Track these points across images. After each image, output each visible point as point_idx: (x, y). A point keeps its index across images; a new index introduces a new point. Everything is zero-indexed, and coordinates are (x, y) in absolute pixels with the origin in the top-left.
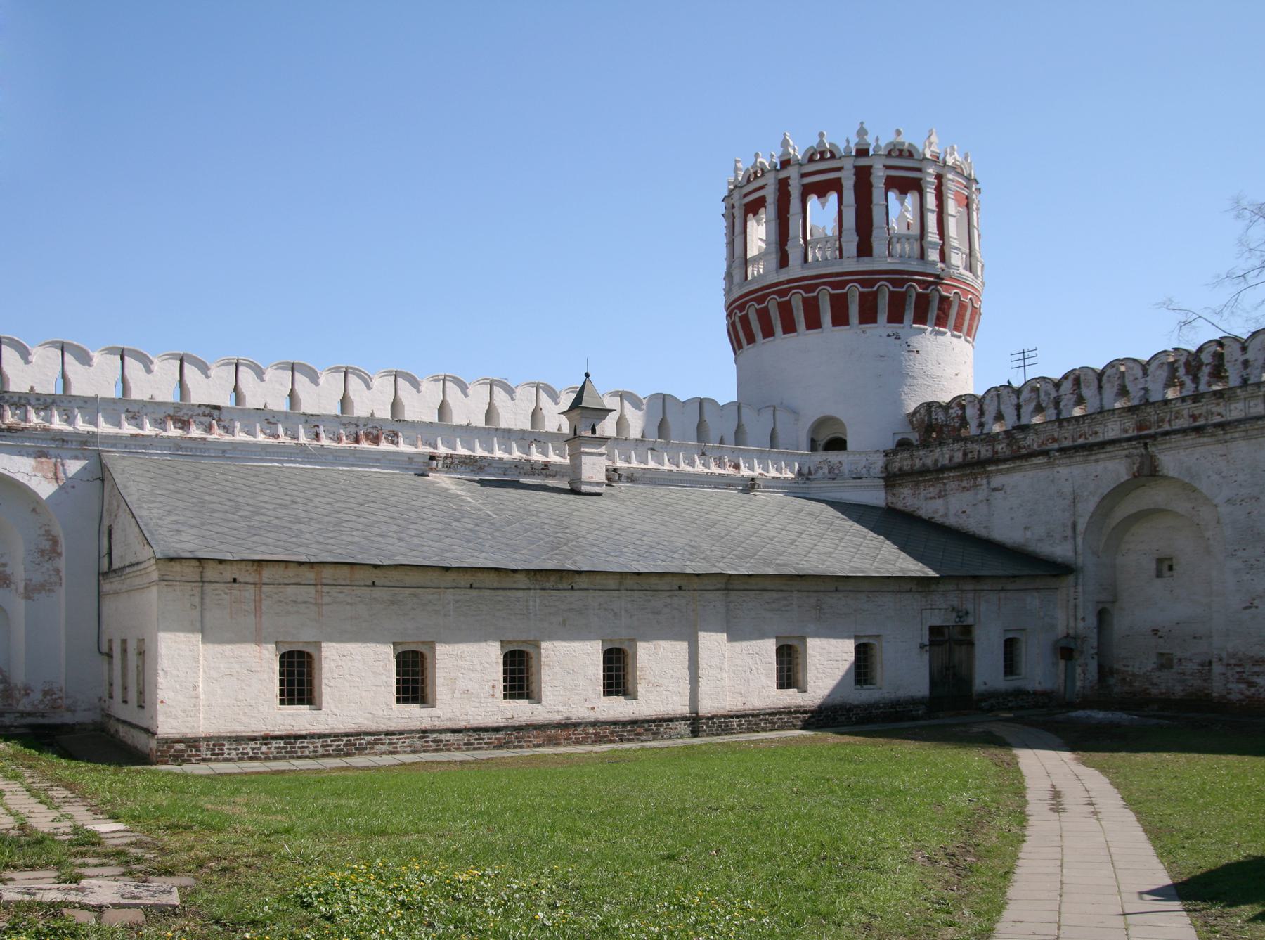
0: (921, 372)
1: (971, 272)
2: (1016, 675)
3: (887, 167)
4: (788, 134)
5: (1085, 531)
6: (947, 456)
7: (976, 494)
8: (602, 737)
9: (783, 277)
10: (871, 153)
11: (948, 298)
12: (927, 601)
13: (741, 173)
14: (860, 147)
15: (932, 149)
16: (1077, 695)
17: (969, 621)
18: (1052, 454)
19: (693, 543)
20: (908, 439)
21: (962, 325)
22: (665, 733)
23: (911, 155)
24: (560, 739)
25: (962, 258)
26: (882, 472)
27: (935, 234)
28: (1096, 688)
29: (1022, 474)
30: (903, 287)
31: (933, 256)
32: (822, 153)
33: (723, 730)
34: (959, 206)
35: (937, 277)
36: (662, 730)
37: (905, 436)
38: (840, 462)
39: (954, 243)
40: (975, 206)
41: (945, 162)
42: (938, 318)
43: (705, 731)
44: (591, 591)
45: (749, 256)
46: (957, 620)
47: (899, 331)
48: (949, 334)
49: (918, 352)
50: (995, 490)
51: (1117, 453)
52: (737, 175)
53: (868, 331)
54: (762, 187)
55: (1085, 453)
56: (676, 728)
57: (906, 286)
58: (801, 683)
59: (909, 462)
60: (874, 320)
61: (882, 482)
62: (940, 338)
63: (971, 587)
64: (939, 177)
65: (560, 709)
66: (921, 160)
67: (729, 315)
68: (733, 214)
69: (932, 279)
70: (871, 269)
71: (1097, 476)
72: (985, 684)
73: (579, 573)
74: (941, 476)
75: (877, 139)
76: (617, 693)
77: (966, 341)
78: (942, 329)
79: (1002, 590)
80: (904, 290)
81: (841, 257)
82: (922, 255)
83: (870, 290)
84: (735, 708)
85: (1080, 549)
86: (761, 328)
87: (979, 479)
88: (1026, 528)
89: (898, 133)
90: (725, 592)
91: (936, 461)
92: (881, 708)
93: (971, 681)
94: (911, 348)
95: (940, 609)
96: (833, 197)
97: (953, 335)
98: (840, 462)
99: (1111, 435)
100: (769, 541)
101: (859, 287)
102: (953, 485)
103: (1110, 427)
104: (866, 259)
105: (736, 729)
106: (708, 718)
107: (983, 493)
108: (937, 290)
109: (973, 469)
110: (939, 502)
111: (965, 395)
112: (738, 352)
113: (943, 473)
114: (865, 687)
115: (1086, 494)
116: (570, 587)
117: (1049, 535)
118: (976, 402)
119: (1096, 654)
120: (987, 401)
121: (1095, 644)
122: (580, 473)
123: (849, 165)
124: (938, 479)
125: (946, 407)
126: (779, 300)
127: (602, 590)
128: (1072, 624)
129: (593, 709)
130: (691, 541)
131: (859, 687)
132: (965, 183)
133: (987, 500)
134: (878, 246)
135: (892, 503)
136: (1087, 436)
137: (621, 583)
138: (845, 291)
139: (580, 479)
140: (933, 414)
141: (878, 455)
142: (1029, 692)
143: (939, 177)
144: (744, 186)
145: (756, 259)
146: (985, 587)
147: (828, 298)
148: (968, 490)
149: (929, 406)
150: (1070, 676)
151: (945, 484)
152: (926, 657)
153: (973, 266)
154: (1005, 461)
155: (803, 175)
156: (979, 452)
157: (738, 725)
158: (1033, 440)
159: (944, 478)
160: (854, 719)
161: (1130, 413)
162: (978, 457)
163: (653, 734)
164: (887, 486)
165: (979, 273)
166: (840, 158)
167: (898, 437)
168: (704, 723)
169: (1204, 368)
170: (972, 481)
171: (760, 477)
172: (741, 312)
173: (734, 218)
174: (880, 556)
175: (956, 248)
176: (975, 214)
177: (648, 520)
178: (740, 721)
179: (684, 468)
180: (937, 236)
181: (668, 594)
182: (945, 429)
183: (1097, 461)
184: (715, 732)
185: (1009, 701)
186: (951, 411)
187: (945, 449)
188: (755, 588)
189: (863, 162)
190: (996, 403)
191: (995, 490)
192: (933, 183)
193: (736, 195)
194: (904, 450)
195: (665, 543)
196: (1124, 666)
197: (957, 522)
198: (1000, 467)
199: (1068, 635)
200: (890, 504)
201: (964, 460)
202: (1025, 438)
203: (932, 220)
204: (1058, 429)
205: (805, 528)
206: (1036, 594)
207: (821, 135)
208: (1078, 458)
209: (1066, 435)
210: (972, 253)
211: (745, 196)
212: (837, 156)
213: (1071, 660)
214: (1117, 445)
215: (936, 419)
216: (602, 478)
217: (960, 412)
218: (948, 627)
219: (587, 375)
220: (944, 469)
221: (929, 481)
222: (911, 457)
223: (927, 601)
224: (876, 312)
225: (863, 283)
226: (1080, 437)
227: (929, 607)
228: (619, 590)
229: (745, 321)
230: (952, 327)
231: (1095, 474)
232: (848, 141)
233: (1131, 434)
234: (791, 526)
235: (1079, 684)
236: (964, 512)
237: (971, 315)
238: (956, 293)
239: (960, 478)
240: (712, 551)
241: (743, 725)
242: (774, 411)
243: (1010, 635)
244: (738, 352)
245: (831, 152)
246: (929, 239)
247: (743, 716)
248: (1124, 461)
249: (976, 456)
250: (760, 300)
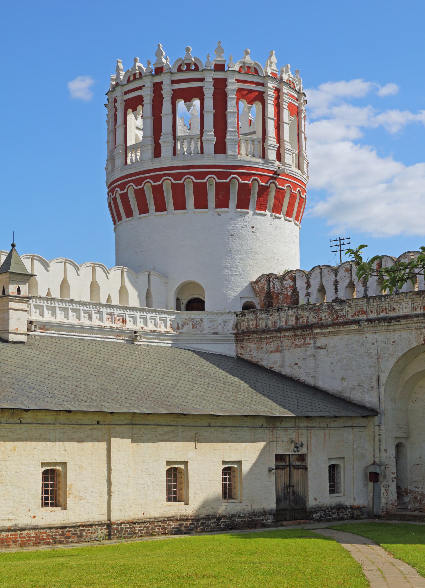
1: (299, 169)
2: (337, 493)
3: (238, 81)
4: (161, 45)
5: (386, 383)
6: (283, 319)
7: (306, 351)
8: (41, 540)
9: (156, 165)
10: (226, 68)
12: (273, 435)
13: (123, 73)
15: (272, 67)
16: (382, 509)
17: (303, 451)
18: (362, 323)
19: (103, 387)
20: (252, 302)
21: (293, 212)
22: (87, 536)
24: (9, 542)
25: (293, 157)
27: (273, 138)
28: (396, 504)
29: (341, 337)
31: (272, 155)
32: (188, 65)
33: (128, 534)
34: (292, 115)
36: (84, 534)
38: (201, 320)
39: (287, 146)
40: (303, 115)
41: (281, 79)
42: (275, 205)
43: (115, 535)
44: (34, 425)
45: (128, 145)
46: (296, 449)
48: (283, 218)
50: (319, 348)
51: (409, 325)
52: (118, 75)
53: (222, 214)
54: (140, 88)
55: (386, 324)
56: (94, 533)
58: (184, 497)
59: (254, 322)
60: (205, 206)
61: (233, 337)
63: (304, 425)
64: (278, 90)
65: (10, 518)
67: (111, 191)
68: (115, 107)
70: (225, 164)
71: (395, 342)
72: (316, 500)
73: (27, 410)
74: (279, 335)
76: (52, 505)
77: (295, 224)
79: (327, 427)
81: (202, 153)
82: (264, 156)
84: (137, 517)
85: (382, 397)
86: (138, 205)
87: (308, 339)
88: (343, 379)
90: (131, 426)
91: (275, 323)
92: (241, 517)
93: (305, 497)
95: (283, 441)
96: (197, 102)
97: (286, 220)
98: (201, 320)
99: (404, 312)
100: (157, 386)
102: (288, 342)
103: (404, 305)
104: (221, 156)
105: (138, 533)
106: (118, 525)
107: (311, 350)
109: (304, 331)
110: (278, 355)
111: (296, 270)
112: (118, 223)
113: (281, 333)
114: (230, 501)
115: (386, 355)
116: (19, 421)
117: (360, 385)
118: (304, 277)
119: (395, 478)
120: (312, 277)
121: (394, 470)
122: (8, 325)
124: (276, 337)
125: (281, 279)
126: (153, 184)
127: (43, 424)
128: (377, 454)
129: (34, 517)
130: (101, 385)
131: (225, 501)
132: (296, 96)
133: (314, 356)
135: (241, 354)
136: (387, 311)
137: (55, 419)
138: (205, 181)
139: (8, 330)
140: (271, 283)
141: (230, 315)
142: (347, 507)
143: (278, 90)
144: (125, 85)
145: (135, 147)
146: (314, 425)
147: (191, 185)
148: (299, 347)
149: (269, 278)
150: (376, 495)
151: (281, 341)
152: (273, 478)
153: (301, 164)
154: (327, 326)
155: (174, 82)
156: (308, 317)
157: (139, 530)
158: (348, 311)
159: (281, 337)
160: (222, 526)
161: (418, 296)
162: (307, 322)
163: (78, 537)
164: (237, 341)
165: (305, 170)
166: (203, 71)
167: (244, 301)
168: (115, 529)
170: (303, 341)
171: (141, 330)
172: (121, 191)
173: (116, 110)
174: (238, 399)
175: (289, 150)
176: (303, 121)
177: (65, 366)
178: (140, 527)
179: (85, 321)
180: (275, 140)
181: (90, 427)
182: (281, 296)
183: (395, 330)
184: (122, 536)
185: (333, 513)
186: (285, 282)
187: (282, 314)
188: (152, 423)
189: (220, 75)
190: (319, 279)
191: (319, 348)
193: (119, 92)
194: (251, 313)
195: (83, 387)
196: (416, 487)
197: (291, 371)
198: (323, 331)
199: (374, 463)
200: (239, 355)
201: (296, 324)
202: (342, 309)
203: (271, 125)
204: (366, 305)
205: (181, 375)
206: (350, 430)
208: (381, 327)
209: (372, 309)
210: (300, 154)
211: (126, 93)
212: (200, 69)
213: (378, 482)
214: (409, 320)
215: (274, 288)
216: (24, 329)
217: (292, 284)
218: (289, 455)
219: (13, 245)
220: (280, 330)
221: (270, 338)
222: (256, 318)
223: (273, 435)
225: (219, 175)
226: (383, 311)
227: (275, 439)
228: (54, 424)
229: (125, 198)
230: (285, 213)
231: (393, 340)
233: (418, 312)
234: (170, 372)
235: (383, 501)
236: (296, 364)
237: (299, 203)
238: (288, 186)
239: (294, 337)
240: (118, 393)
241: (143, 530)
242: (149, 275)
243: (333, 462)
244: (118, 223)
245: (195, 65)
246: (269, 142)
247: (143, 523)
248: (414, 332)
249: (305, 321)
250: (138, 182)
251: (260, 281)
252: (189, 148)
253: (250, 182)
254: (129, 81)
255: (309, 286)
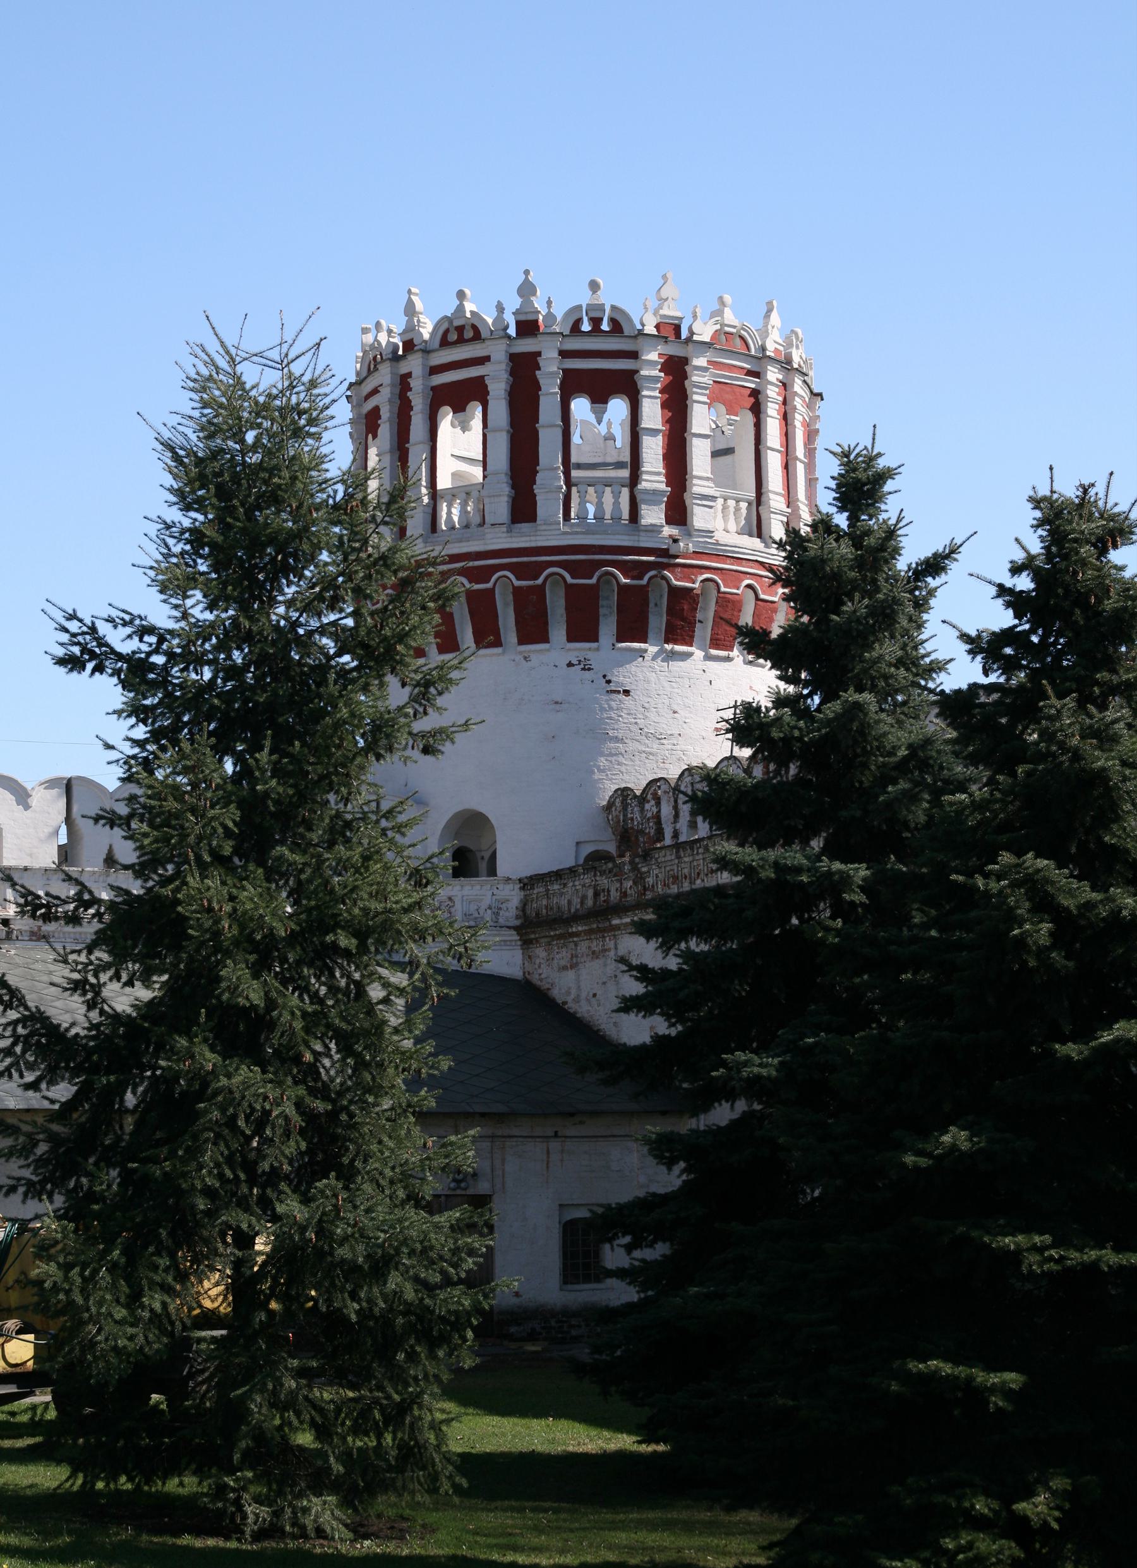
0: (634, 728)
11: (690, 590)
14: (522, 318)
23: (617, 327)
26: (517, 917)
30: (591, 578)
32: (596, 322)
35: (664, 553)
37: (600, 847)
38: (450, 899)
46: (452, 1185)
47: (589, 655)
49: (627, 692)
53: (533, 657)
57: (597, 574)
60: (542, 637)
62: (677, 666)
66: (635, 337)
69: (652, 558)
70: (533, 544)
75: (549, 303)
78: (679, 648)
80: (593, 581)
83: (531, 583)
89: (594, 286)
94: (612, 687)
96: (618, 408)
97: (708, 658)
98: (450, 899)
101: (512, 577)
104: (525, 527)
108: (664, 578)
110: (571, 974)
123: (498, 352)
126: (517, 583)
134: (548, 505)
138: (489, 585)
155: (435, 370)
169: (734, 754)
189: (526, 346)
192: (655, 379)
197: (588, 1011)
207: (461, 295)
217: (655, 810)
224: (546, 623)
225: (521, 571)
232: (500, 308)
251: (614, 803)
252: (599, 506)
253: (697, 585)
254: (445, 343)
255: (677, 816)
